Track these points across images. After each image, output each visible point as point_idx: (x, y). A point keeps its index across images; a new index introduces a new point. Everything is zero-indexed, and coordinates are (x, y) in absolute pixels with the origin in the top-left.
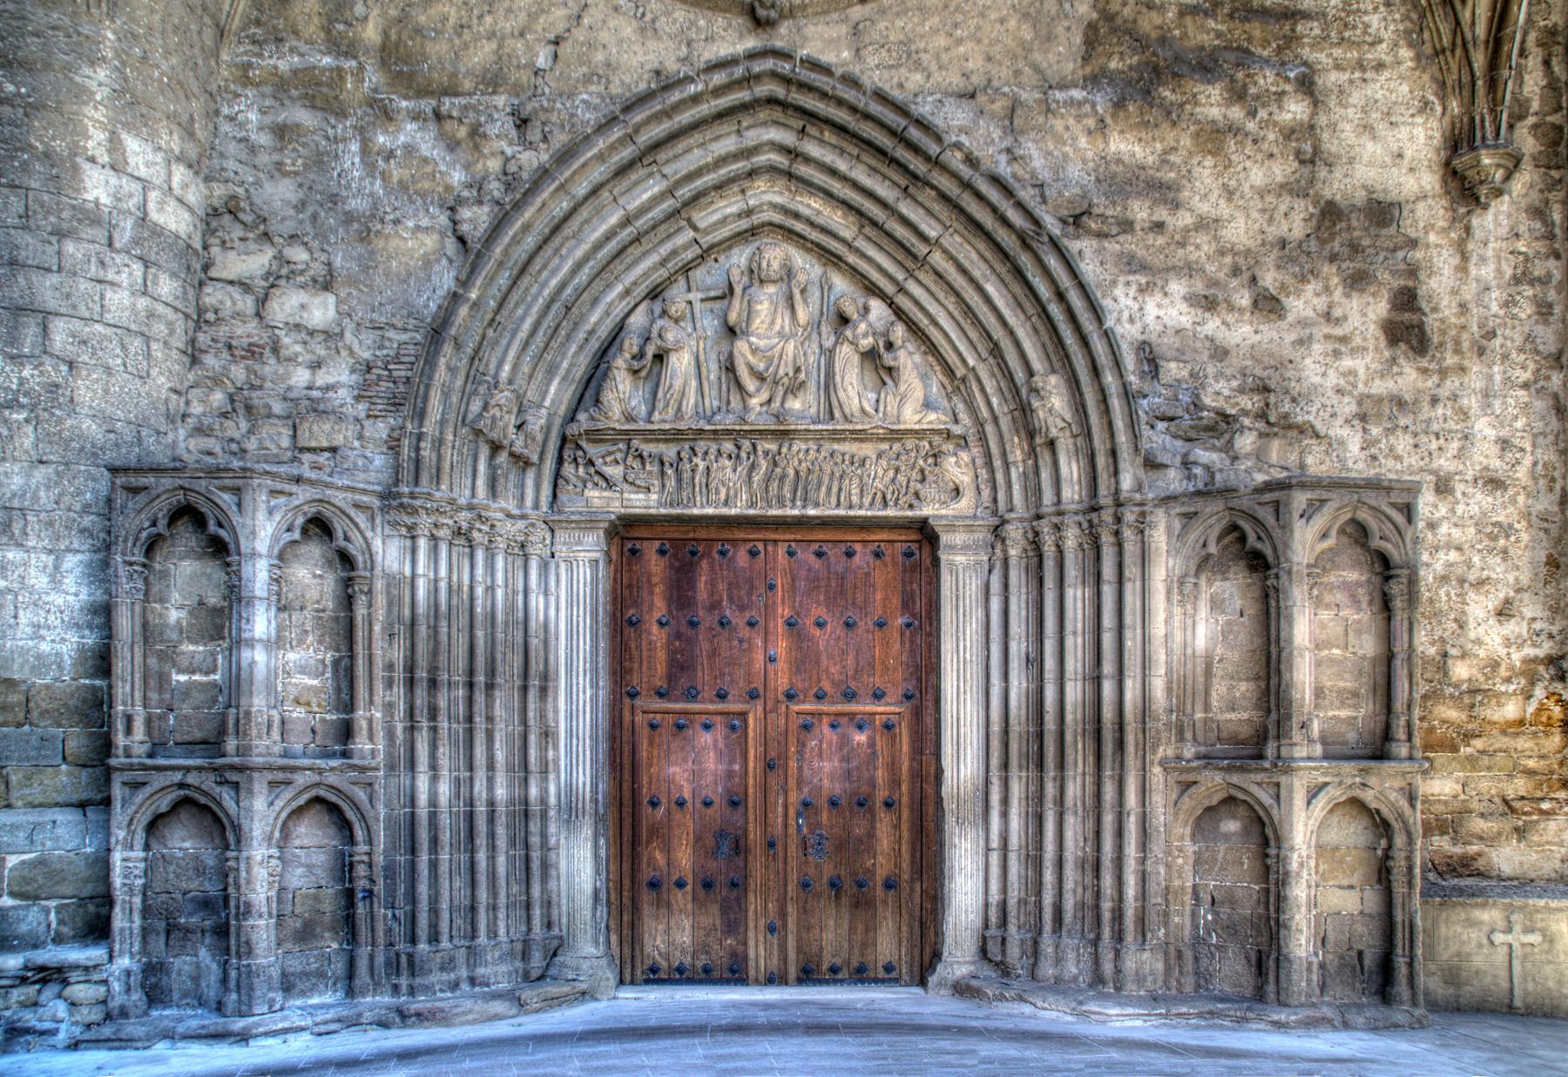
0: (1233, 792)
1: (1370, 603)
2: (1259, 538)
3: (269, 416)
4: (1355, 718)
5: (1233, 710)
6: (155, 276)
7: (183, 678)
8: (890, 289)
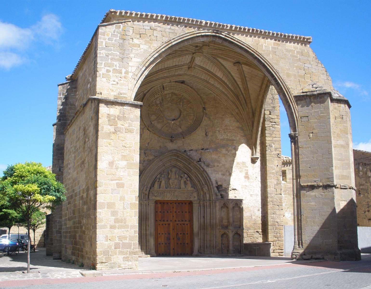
8: (187, 174)
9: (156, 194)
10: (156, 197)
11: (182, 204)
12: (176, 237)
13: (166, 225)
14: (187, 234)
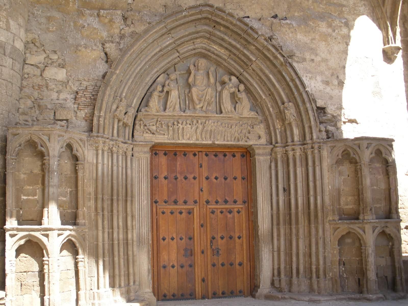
0: (351, 230)
1: (383, 173)
2: (354, 154)
3: (46, 109)
4: (381, 207)
5: (347, 205)
6: (15, 64)
7: (25, 198)
8: (238, 74)
9: (154, 128)
10: (153, 134)
11: (225, 155)
12: (209, 247)
13: (181, 213)
14: (239, 238)
